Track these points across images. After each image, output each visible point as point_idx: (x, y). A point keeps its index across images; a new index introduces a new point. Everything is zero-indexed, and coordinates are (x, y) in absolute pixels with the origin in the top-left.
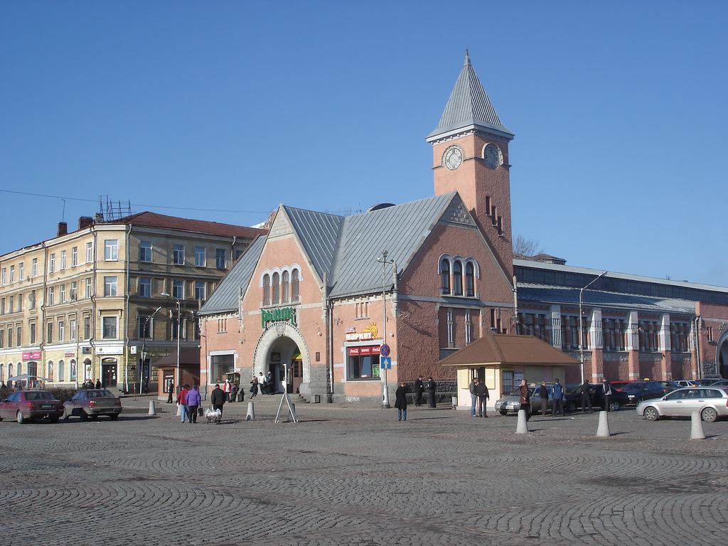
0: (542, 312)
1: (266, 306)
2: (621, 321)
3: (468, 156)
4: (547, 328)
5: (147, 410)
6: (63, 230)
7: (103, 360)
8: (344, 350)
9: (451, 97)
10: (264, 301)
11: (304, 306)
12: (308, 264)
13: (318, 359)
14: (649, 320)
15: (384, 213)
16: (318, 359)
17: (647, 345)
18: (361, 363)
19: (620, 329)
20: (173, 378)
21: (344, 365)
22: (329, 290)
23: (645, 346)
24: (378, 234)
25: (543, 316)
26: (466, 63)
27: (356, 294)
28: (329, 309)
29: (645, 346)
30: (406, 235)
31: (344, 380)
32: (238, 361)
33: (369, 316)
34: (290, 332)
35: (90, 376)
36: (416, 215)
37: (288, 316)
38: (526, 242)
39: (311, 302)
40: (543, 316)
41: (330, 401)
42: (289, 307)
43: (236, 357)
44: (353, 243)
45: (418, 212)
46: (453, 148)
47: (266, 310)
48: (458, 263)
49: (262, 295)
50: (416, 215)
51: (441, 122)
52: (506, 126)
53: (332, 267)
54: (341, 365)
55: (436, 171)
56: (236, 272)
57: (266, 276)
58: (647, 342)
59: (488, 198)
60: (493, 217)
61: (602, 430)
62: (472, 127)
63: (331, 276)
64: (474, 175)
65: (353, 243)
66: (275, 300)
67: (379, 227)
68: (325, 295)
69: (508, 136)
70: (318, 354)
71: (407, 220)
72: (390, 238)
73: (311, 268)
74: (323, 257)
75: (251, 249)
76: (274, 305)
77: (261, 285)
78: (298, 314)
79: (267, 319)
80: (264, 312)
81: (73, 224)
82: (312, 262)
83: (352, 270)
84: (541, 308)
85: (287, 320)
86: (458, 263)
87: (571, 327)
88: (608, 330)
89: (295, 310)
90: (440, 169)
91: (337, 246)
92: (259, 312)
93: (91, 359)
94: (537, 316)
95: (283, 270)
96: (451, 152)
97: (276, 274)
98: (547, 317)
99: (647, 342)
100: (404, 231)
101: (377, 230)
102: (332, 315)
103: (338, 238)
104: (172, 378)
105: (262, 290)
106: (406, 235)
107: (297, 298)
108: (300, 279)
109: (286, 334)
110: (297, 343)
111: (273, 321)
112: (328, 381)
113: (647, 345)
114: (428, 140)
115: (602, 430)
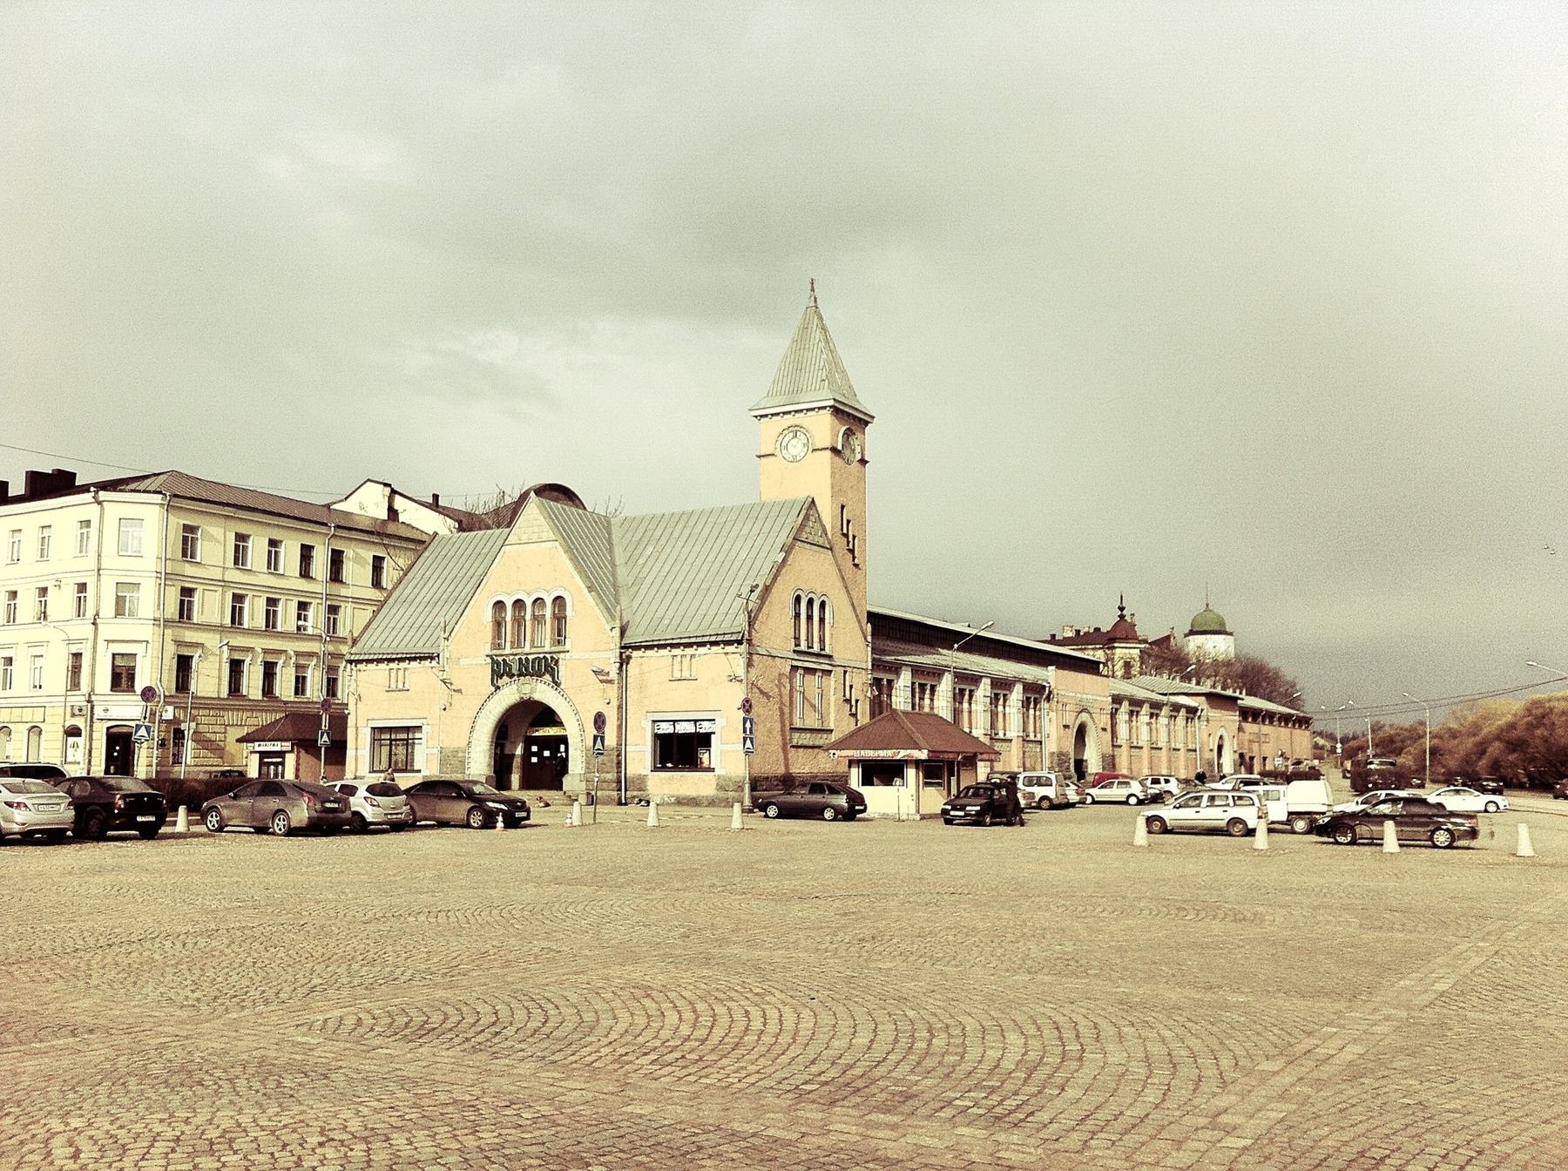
0: (891, 677)
2: (305, 615)
7: (108, 728)
14: (999, 692)
20: (283, 764)
27: (699, 640)
28: (624, 661)
34: (541, 691)
37: (545, 667)
46: (795, 430)
47: (500, 659)
48: (810, 602)
52: (865, 402)
59: (843, 507)
60: (846, 536)
62: (831, 403)
66: (517, 643)
86: (810, 602)
93: (82, 726)
96: (791, 435)
102: (627, 671)
104: (276, 764)
109: (537, 697)
111: (511, 676)
112: (619, 772)
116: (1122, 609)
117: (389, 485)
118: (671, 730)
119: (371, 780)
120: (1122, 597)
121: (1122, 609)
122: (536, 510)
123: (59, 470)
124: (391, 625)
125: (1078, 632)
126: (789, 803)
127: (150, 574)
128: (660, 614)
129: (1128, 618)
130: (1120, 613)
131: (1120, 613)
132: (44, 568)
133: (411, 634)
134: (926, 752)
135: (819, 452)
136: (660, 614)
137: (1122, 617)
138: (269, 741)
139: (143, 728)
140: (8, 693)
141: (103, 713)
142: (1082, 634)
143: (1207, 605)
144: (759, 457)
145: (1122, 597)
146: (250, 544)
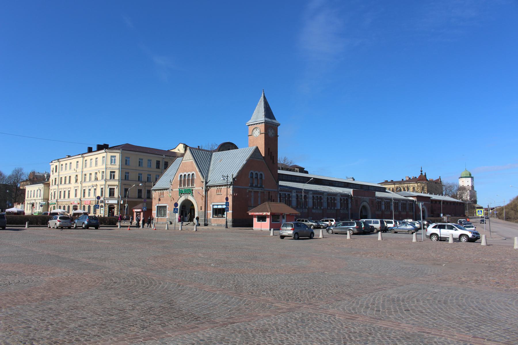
1: (180, 187)
3: (262, 132)
4: (291, 199)
5: (319, 236)
6: (90, 150)
8: (211, 206)
9: (256, 108)
10: (180, 185)
11: (196, 188)
12: (198, 172)
13: (201, 209)
15: (231, 152)
16: (201, 209)
17: (317, 206)
18: (219, 212)
19: (320, 200)
21: (211, 212)
22: (206, 183)
23: (316, 206)
24: (226, 161)
25: (289, 195)
26: (263, 95)
28: (206, 191)
29: (316, 206)
30: (237, 162)
31: (211, 217)
32: (168, 209)
33: (222, 193)
34: (190, 198)
35: (40, 211)
36: (241, 154)
37: (190, 192)
38: (455, 183)
39: (198, 187)
40: (289, 195)
41: (206, 225)
42: (190, 188)
43: (167, 207)
44: (216, 164)
45: (242, 153)
47: (181, 189)
49: (179, 183)
50: (241, 154)
51: (252, 118)
53: (208, 173)
54: (210, 212)
55: (250, 137)
56: (167, 173)
57: (181, 175)
58: (317, 204)
61: (379, 238)
62: (264, 121)
63: (207, 177)
64: (264, 139)
65: (216, 164)
67: (226, 158)
68: (205, 184)
69: (278, 124)
70: (201, 207)
71: (237, 156)
72: (230, 163)
73: (199, 174)
74: (204, 170)
75: (173, 163)
76: (184, 187)
77: (179, 179)
78: (194, 191)
79: (181, 193)
80: (180, 190)
81: (95, 148)
82: (200, 171)
83: (215, 175)
84: (288, 191)
85: (190, 194)
87: (316, 200)
88: (315, 200)
89: (193, 190)
90: (251, 136)
91: (210, 165)
92: (178, 190)
94: (287, 194)
95: (188, 173)
97: (185, 175)
98: (291, 195)
99: (317, 204)
100: (236, 161)
101: (225, 159)
103: (210, 161)
105: (179, 181)
106: (237, 162)
107: (194, 185)
108: (195, 178)
109: (189, 199)
110: (192, 201)
111: (183, 194)
112: (205, 218)
113: (317, 206)
114: (247, 124)
115: (379, 238)
116: (421, 171)
117: (185, 144)
118: (217, 207)
119: (67, 225)
120: (421, 168)
121: (421, 171)
122: (189, 152)
123: (104, 144)
124: (162, 181)
125: (410, 178)
126: (479, 209)
127: (117, 169)
128: (216, 178)
129: (424, 174)
130: (421, 172)
131: (421, 172)
132: (96, 168)
133: (165, 183)
134: (269, 213)
135: (262, 134)
136: (216, 178)
137: (422, 174)
138: (138, 209)
139: (97, 206)
140: (89, 198)
141: (107, 202)
142: (411, 179)
143: (466, 169)
144: (249, 136)
145: (421, 168)
146: (143, 161)
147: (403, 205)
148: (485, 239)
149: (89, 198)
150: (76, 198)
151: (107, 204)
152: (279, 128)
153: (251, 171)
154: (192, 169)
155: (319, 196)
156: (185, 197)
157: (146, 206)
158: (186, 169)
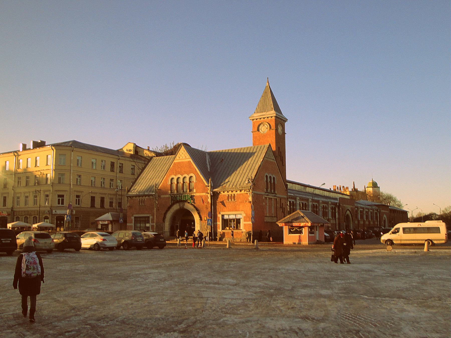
57: (172, 179)
64: (274, 137)
81: (30, 145)
95: (184, 176)
117: (135, 144)
134: (310, 223)
147: (314, 208)
148: (102, 220)
149: (26, 207)
150: (5, 207)
151: (55, 215)
152: (286, 124)
153: (266, 174)
154: (190, 171)
155: (304, 202)
156: (179, 205)
157: (123, 217)
158: (179, 170)
